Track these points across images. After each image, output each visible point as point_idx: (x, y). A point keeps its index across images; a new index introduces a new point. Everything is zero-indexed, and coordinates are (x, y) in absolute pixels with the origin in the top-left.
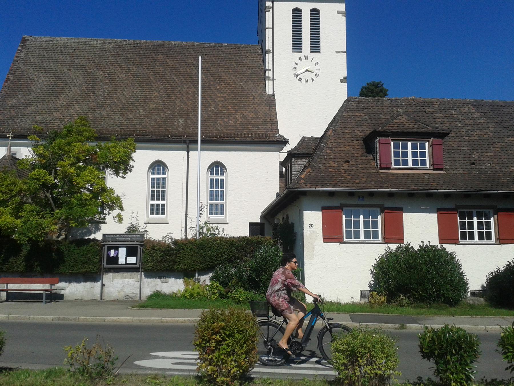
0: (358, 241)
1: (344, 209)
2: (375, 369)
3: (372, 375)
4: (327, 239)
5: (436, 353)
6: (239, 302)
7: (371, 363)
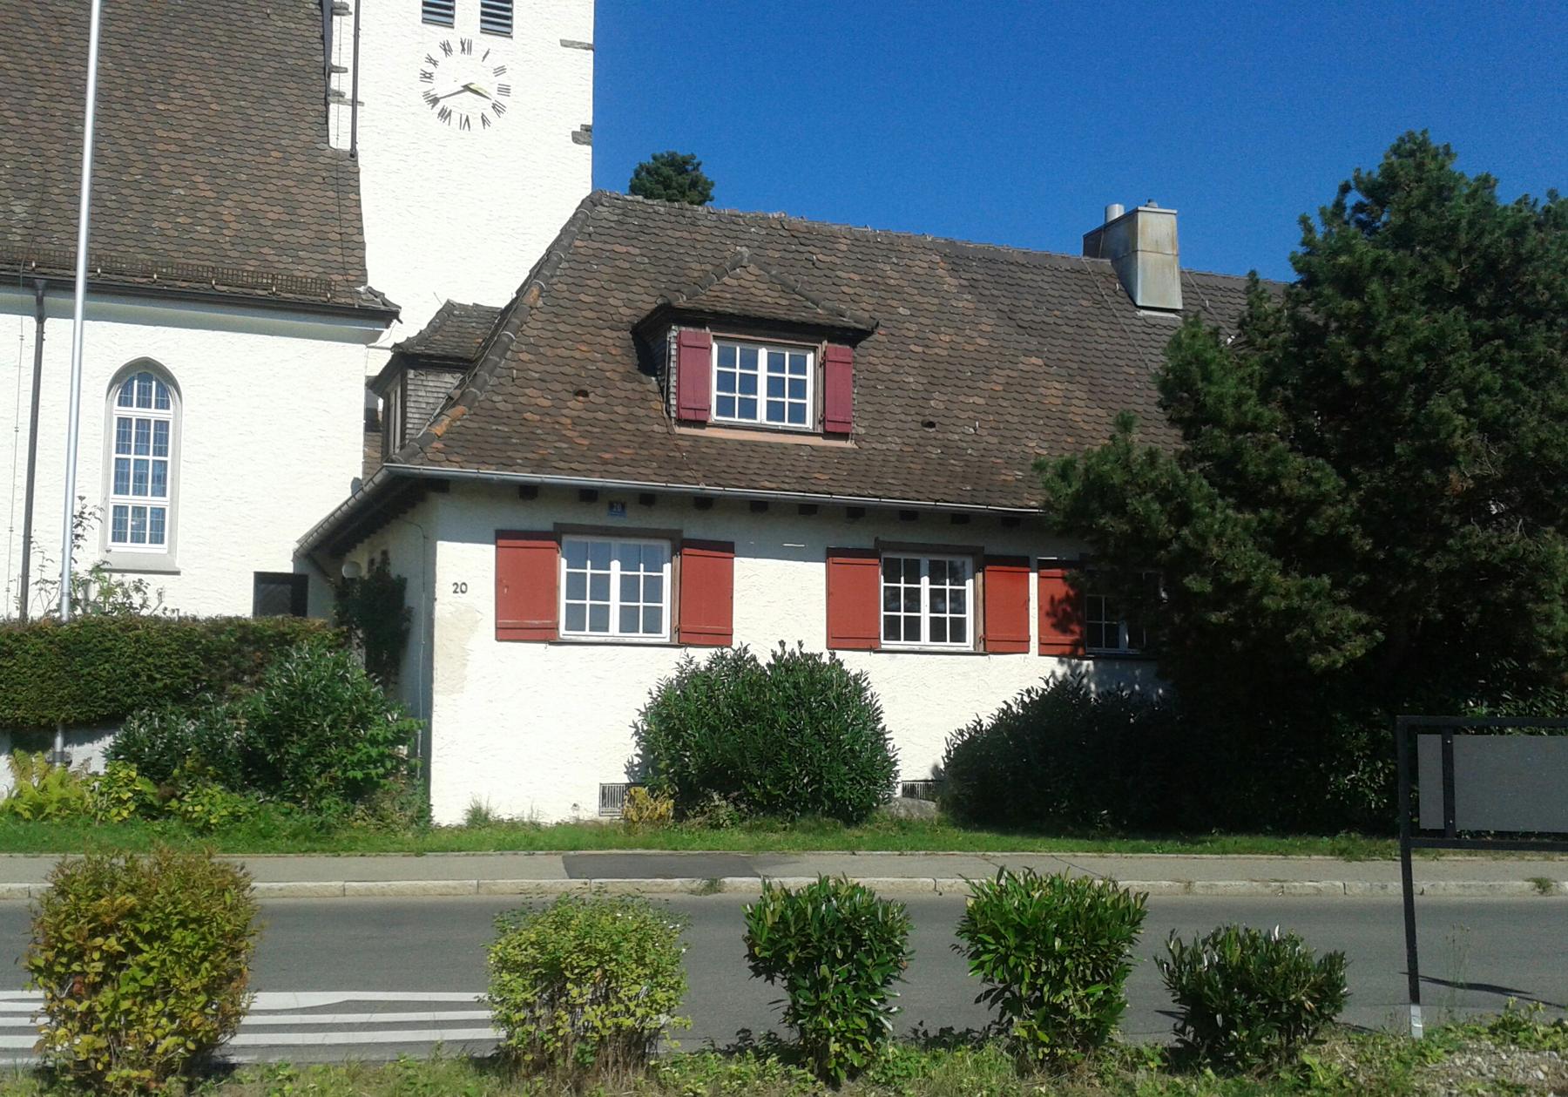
0: (602, 640)
1: (566, 539)
2: (615, 1015)
3: (606, 1033)
4: (506, 632)
5: (791, 957)
6: (205, 830)
7: (606, 997)
